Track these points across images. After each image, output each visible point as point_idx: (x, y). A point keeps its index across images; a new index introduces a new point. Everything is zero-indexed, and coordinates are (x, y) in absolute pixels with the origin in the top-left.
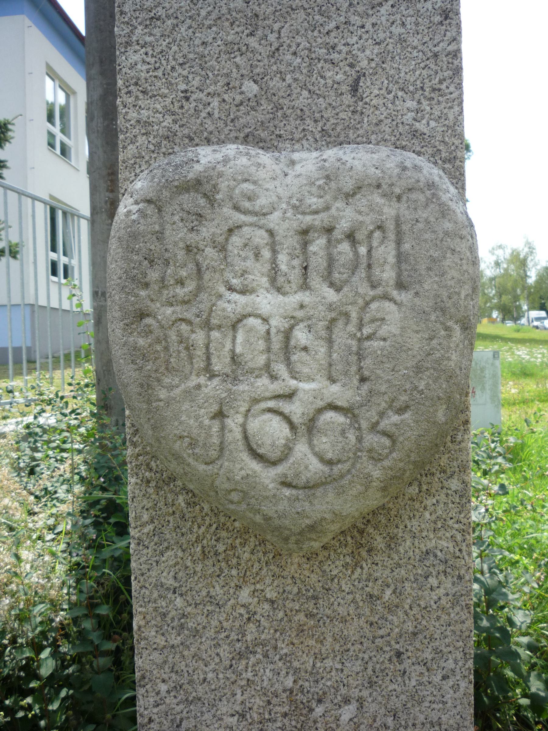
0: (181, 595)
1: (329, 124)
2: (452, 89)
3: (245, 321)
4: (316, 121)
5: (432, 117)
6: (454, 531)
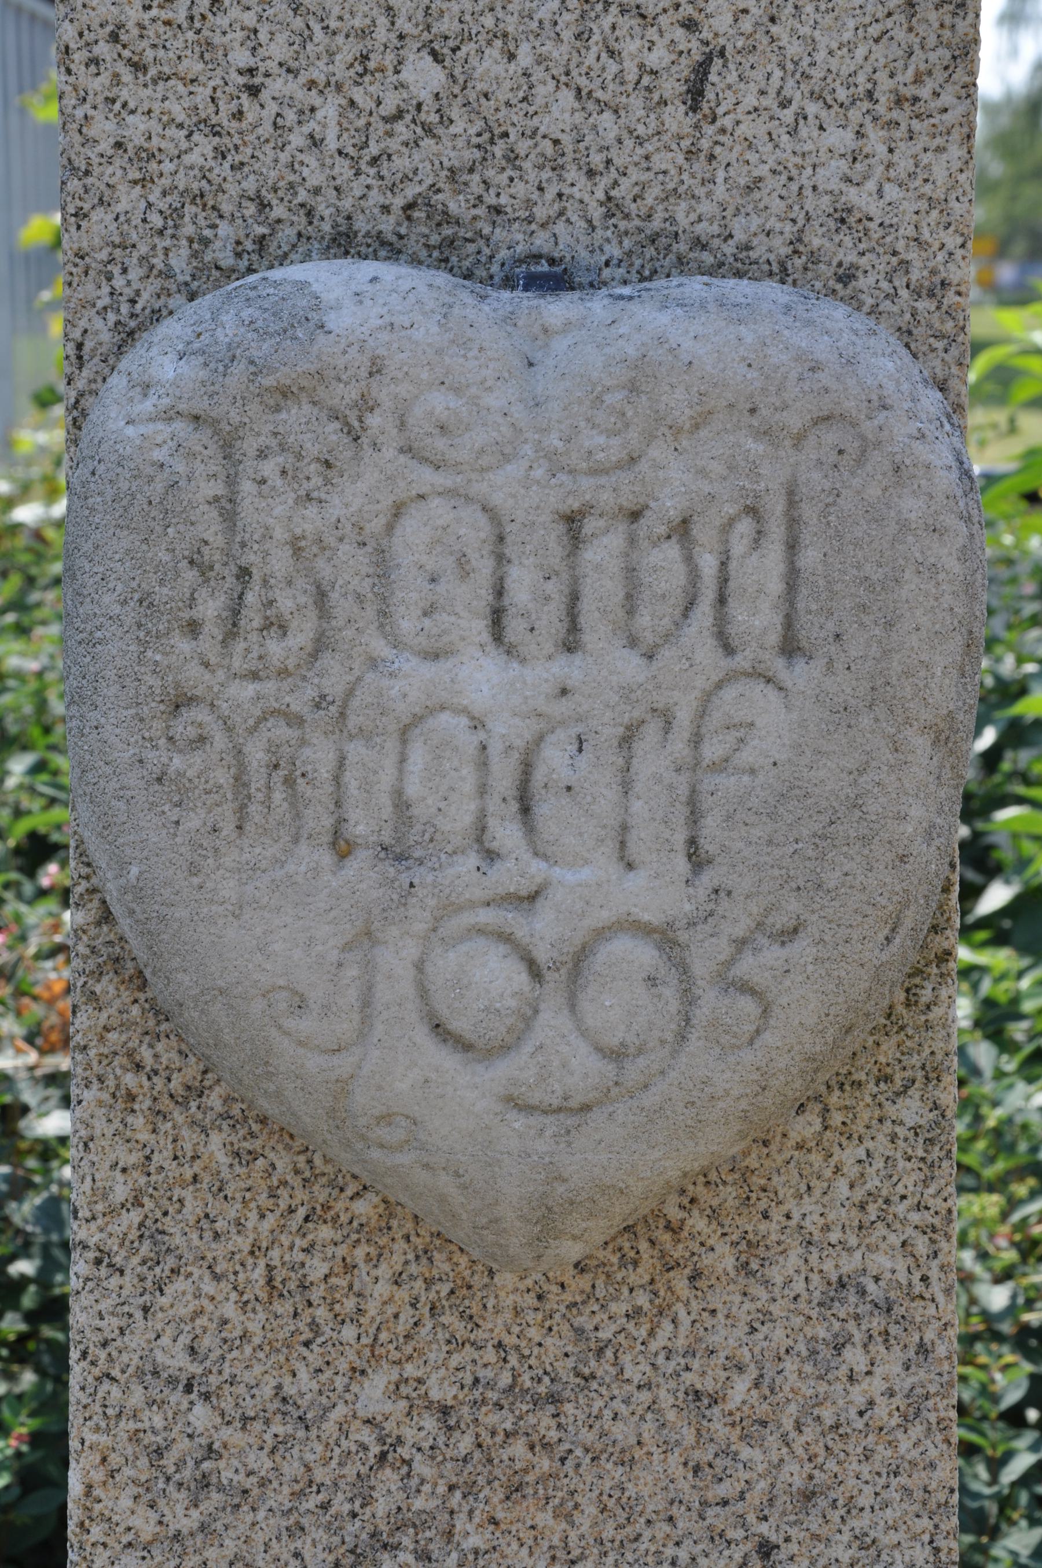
0: (206, 1397)
1: (625, 183)
2: (947, 99)
3: (431, 723)
4: (591, 173)
5: (892, 174)
6: (910, 1231)
